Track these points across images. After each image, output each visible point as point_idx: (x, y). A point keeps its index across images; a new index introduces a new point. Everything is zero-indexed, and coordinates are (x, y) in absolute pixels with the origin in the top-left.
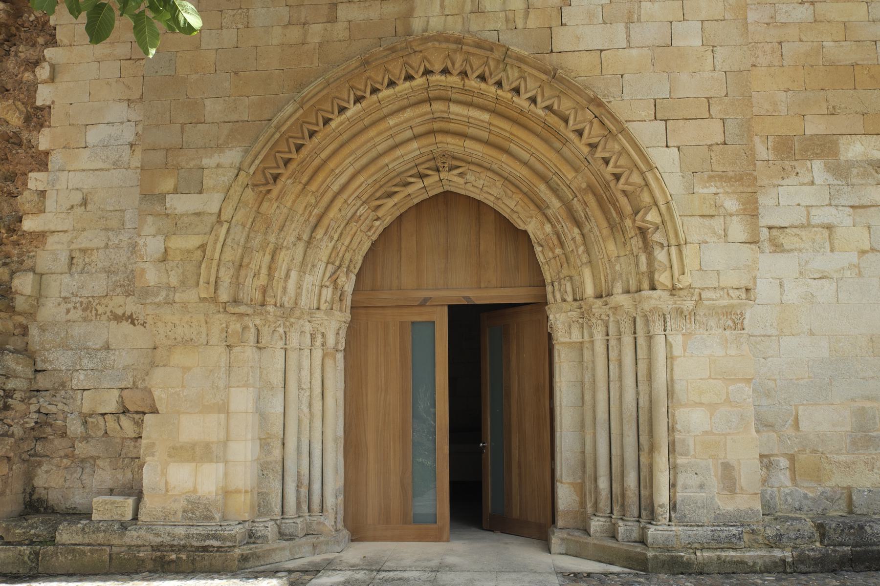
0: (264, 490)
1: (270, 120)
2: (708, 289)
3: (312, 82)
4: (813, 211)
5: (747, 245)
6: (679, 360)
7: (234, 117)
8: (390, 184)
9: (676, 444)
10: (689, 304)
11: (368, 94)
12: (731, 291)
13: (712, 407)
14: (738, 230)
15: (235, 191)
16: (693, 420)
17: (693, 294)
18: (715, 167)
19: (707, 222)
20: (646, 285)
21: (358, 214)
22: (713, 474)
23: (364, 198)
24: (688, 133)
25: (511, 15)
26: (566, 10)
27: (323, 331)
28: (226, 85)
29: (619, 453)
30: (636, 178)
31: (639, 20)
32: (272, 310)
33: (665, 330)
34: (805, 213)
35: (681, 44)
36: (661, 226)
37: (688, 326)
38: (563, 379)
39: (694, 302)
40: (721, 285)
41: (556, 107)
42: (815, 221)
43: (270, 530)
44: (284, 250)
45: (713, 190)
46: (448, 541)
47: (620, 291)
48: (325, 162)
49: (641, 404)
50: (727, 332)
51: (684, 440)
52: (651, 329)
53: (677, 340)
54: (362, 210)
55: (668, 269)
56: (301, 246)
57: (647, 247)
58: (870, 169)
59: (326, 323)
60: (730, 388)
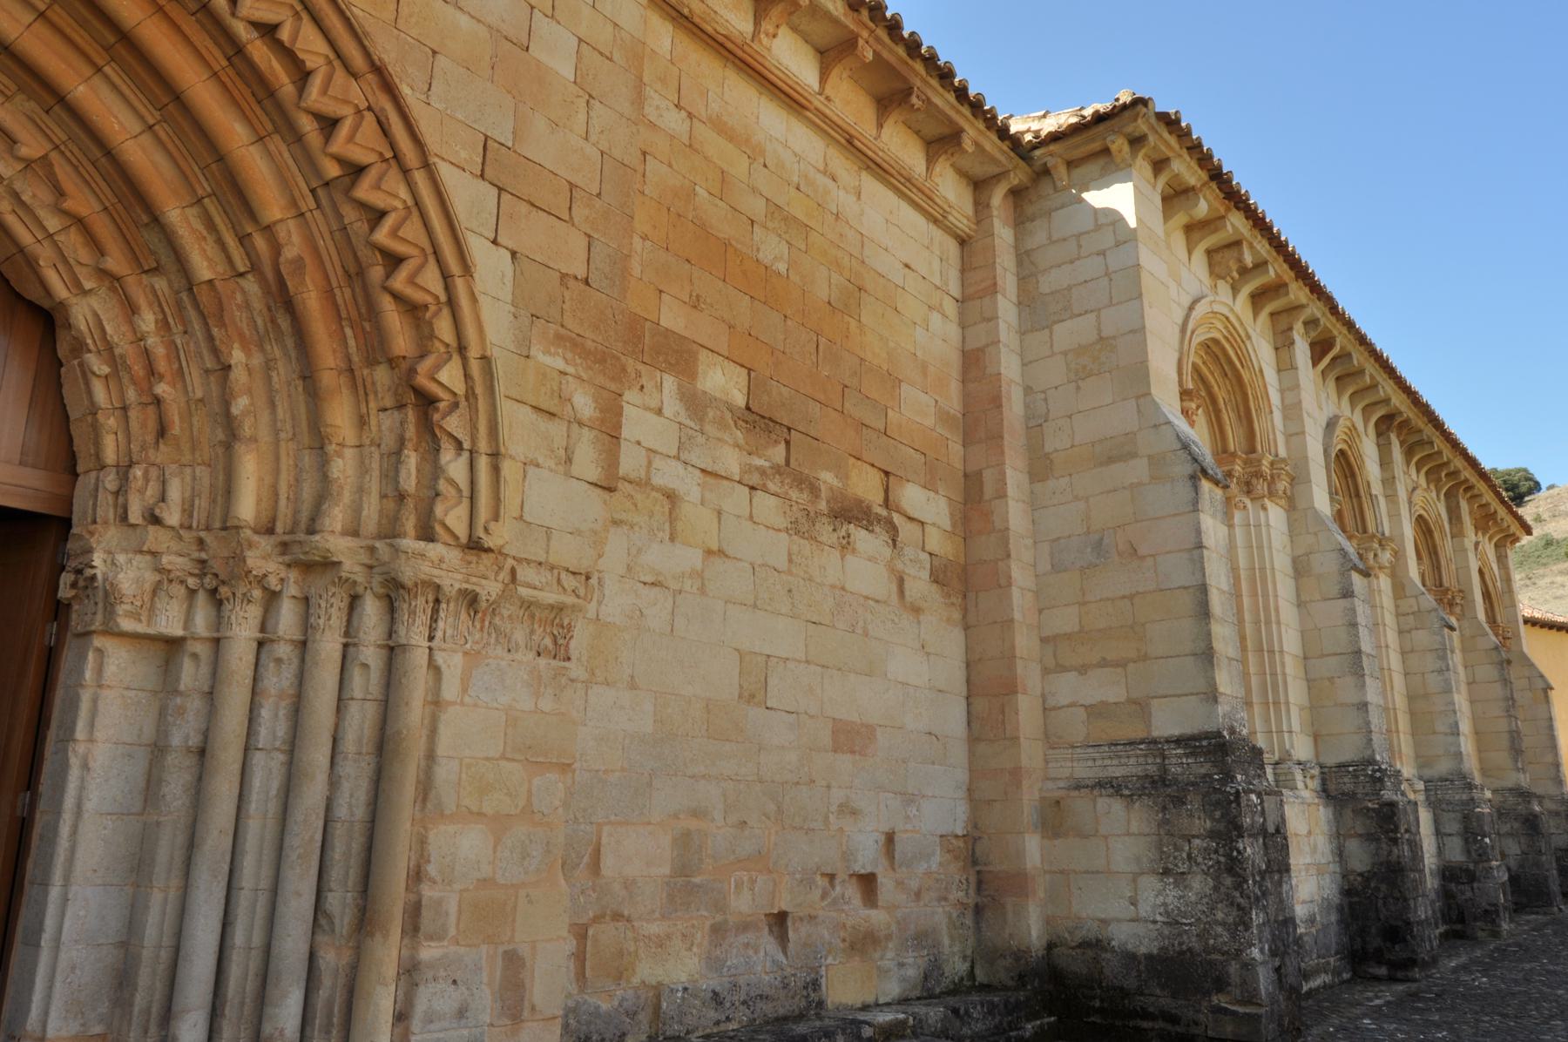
2: (528, 561)
4: (658, 462)
5: (599, 491)
6: (451, 709)
9: (424, 912)
10: (490, 589)
12: (563, 575)
13: (499, 824)
14: (587, 461)
16: (461, 851)
17: (501, 568)
18: (569, 322)
19: (543, 424)
20: (410, 523)
22: (485, 980)
24: (533, 233)
29: (257, 939)
30: (431, 279)
33: (431, 638)
34: (644, 462)
35: (543, 58)
36: (463, 404)
37: (477, 636)
38: (99, 735)
39: (500, 586)
40: (551, 560)
41: (285, 35)
42: (657, 480)
45: (560, 364)
47: (338, 527)
49: (341, 812)
50: (542, 661)
51: (439, 902)
52: (402, 630)
53: (452, 663)
55: (466, 503)
57: (430, 434)
58: (728, 416)
60: (536, 781)
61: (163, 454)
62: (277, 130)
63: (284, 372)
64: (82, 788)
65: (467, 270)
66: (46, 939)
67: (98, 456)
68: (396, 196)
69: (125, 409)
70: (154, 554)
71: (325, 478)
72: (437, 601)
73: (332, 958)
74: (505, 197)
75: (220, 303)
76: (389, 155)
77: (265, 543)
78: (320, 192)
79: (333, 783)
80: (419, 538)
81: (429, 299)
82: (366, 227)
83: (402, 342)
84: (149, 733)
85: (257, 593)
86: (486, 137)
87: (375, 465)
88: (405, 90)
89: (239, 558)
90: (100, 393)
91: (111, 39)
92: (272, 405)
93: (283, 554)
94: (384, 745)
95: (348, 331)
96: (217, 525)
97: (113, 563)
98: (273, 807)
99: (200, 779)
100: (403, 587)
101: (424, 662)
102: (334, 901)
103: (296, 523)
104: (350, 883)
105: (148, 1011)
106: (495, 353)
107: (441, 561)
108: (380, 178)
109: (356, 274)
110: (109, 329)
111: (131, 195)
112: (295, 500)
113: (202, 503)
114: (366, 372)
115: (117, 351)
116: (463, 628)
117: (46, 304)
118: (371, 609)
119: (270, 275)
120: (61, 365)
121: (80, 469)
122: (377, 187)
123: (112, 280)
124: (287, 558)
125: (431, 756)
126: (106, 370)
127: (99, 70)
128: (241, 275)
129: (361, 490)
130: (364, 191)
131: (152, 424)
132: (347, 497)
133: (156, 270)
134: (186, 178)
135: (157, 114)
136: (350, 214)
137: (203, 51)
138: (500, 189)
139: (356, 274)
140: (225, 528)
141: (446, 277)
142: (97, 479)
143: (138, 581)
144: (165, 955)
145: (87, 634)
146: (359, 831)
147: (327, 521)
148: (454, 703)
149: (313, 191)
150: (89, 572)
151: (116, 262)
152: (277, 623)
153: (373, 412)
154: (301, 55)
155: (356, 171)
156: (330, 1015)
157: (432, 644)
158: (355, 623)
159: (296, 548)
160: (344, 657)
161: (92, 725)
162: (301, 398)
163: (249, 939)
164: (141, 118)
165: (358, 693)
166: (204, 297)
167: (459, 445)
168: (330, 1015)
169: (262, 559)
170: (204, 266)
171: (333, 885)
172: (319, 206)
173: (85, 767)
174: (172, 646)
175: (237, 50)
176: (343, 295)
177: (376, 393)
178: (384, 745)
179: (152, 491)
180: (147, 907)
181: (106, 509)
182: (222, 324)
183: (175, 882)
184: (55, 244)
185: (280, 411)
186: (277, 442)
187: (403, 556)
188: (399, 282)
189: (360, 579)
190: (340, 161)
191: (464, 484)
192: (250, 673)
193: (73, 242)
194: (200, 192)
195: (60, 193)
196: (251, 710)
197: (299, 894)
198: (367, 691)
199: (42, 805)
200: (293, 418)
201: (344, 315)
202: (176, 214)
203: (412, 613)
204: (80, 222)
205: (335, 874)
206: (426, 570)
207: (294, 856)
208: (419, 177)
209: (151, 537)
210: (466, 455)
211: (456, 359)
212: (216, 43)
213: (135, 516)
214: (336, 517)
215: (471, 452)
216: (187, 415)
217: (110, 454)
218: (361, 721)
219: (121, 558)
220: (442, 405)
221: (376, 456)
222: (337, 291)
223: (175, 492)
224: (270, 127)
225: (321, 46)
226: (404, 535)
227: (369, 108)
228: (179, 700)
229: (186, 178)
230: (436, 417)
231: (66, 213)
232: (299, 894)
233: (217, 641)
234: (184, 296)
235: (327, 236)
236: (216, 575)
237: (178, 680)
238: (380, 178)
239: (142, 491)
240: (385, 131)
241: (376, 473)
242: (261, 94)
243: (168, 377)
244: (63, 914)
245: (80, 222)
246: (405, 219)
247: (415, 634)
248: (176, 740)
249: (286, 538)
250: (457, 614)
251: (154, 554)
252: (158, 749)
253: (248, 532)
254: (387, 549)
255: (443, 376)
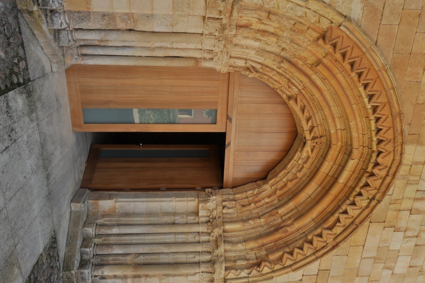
0: (92, 17)
1: (376, 45)
3: (394, 76)
6: (186, 279)
7: (386, 12)
8: (310, 109)
9: (139, 279)
11: (376, 115)
15: (329, 13)
20: (228, 265)
21: (293, 87)
23: (303, 92)
25: (398, 202)
26: (393, 229)
27: (214, 60)
28: (413, 6)
29: (134, 242)
30: (289, 263)
31: (375, 263)
32: (232, 33)
33: (202, 272)
36: (260, 273)
38: (177, 203)
41: (338, 224)
43: (60, 21)
44: (277, 40)
46: (73, 131)
47: (226, 248)
48: (335, 77)
49: (161, 256)
52: (203, 266)
53: (197, 278)
54: (295, 90)
55: (236, 277)
56: (277, 50)
57: (252, 266)
59: (220, 62)
61: (239, 207)
62: (316, 223)
63: (261, 230)
64: (166, 201)
65: (294, 270)
66: (136, 199)
67: (237, 193)
68: (307, 252)
69: (247, 198)
70: (216, 208)
71: (238, 243)
72: (211, 273)
73: (129, 259)
74: (316, 276)
75: (274, 215)
76: (317, 249)
77: (221, 231)
78: (304, 234)
79: (167, 254)
80: (225, 267)
81: (284, 262)
82: (298, 246)
83: (272, 257)
84: (177, 211)
85: (209, 231)
86: (330, 270)
87: (242, 254)
88: (335, 251)
89: (217, 226)
90: (250, 192)
91: (327, 188)
92: (253, 228)
93: (219, 235)
94: (176, 264)
95: (273, 244)
96: (224, 220)
97: (214, 200)
98: (162, 241)
99: (169, 224)
100: (214, 265)
101: (196, 272)
102: (141, 257)
103: (226, 237)
104: (145, 261)
105: (120, 221)
106: (274, 279)
107: (220, 273)
108: (311, 248)
109: (287, 245)
110: (264, 193)
111: (294, 194)
112: (232, 236)
113: (229, 216)
114: (264, 249)
115: (259, 195)
116: (205, 279)
117: (268, 178)
118: (207, 257)
119: (282, 225)
120: (256, 182)
121: (234, 189)
122: (308, 248)
123: (275, 192)
124: (218, 237)
125: (174, 276)
126: (255, 193)
127: (320, 186)
128: (281, 218)
129: (235, 251)
130: (306, 245)
131: (245, 204)
132: (233, 248)
133: (279, 200)
134: (300, 205)
135: (313, 198)
136: (300, 242)
137: (330, 207)
138: (317, 275)
139: (287, 245)
140: (223, 222)
141: (290, 266)
142: (232, 194)
143: (210, 206)
144: (131, 223)
145: (198, 197)
146: (157, 261)
147: (227, 245)
148: (187, 279)
149: (304, 232)
150: (211, 196)
151: (279, 193)
152: (203, 236)
153: (255, 252)
154: (335, 228)
155: (311, 242)
156: (116, 260)
157: (201, 273)
158: (205, 253)
159: (220, 239)
160: (197, 252)
161: (179, 201)
162: (255, 235)
163: (134, 240)
164: (312, 195)
165: (188, 256)
166: (274, 212)
167: (249, 274)
168: (116, 260)
169: (217, 232)
170: (281, 211)
171: (145, 257)
172: (301, 234)
173: (170, 201)
174: (197, 213)
175: (332, 214)
176: (281, 242)
177: (259, 252)
178: (176, 264)
179: (230, 206)
180: (141, 217)
181: (225, 197)
182: (269, 216)
183: (146, 222)
184: (280, 181)
185: (252, 230)
186: (245, 230)
187: (220, 265)
188: (286, 255)
189: (215, 254)
190: (312, 239)
191: (240, 276)
192: (192, 231)
193: (281, 184)
194: (298, 208)
195: (291, 181)
196: (183, 233)
197: (143, 250)
198: (189, 258)
199: (163, 193)
200: (251, 233)
201: (276, 242)
202: (291, 205)
203: (208, 268)
204: (286, 185)
205: (147, 257)
206: (218, 270)
207: (151, 248)
208: (313, 257)
209: (220, 207)
210: (247, 276)
211: (271, 271)
212: (332, 209)
213: (224, 203)
214: (228, 247)
215: (248, 277)
216: (248, 210)
217: (237, 196)
218: (182, 258)
219: (215, 202)
220: (258, 269)
221: (244, 254)
222: (282, 240)
223: (230, 211)
224: (316, 222)
225: (338, 232)
226: (226, 264)
227: (327, 244)
228: (185, 217)
229: (300, 205)
230: (255, 268)
231: (287, 183)
232: (143, 250)
233: (198, 223)
234: (274, 207)
235: (294, 237)
236: (213, 222)
237: (190, 216)
238: (311, 248)
239: (229, 204)
240: (323, 248)
241: (240, 254)
242: (324, 219)
243: (255, 206)
244: (140, 202)
245: (286, 185)
246: (302, 255)
247: (203, 268)
248: (177, 218)
249: (222, 236)
250: (208, 277)
251: (216, 208)
252: (175, 214)
253: (223, 228)
254: (222, 260)
255: (266, 268)
